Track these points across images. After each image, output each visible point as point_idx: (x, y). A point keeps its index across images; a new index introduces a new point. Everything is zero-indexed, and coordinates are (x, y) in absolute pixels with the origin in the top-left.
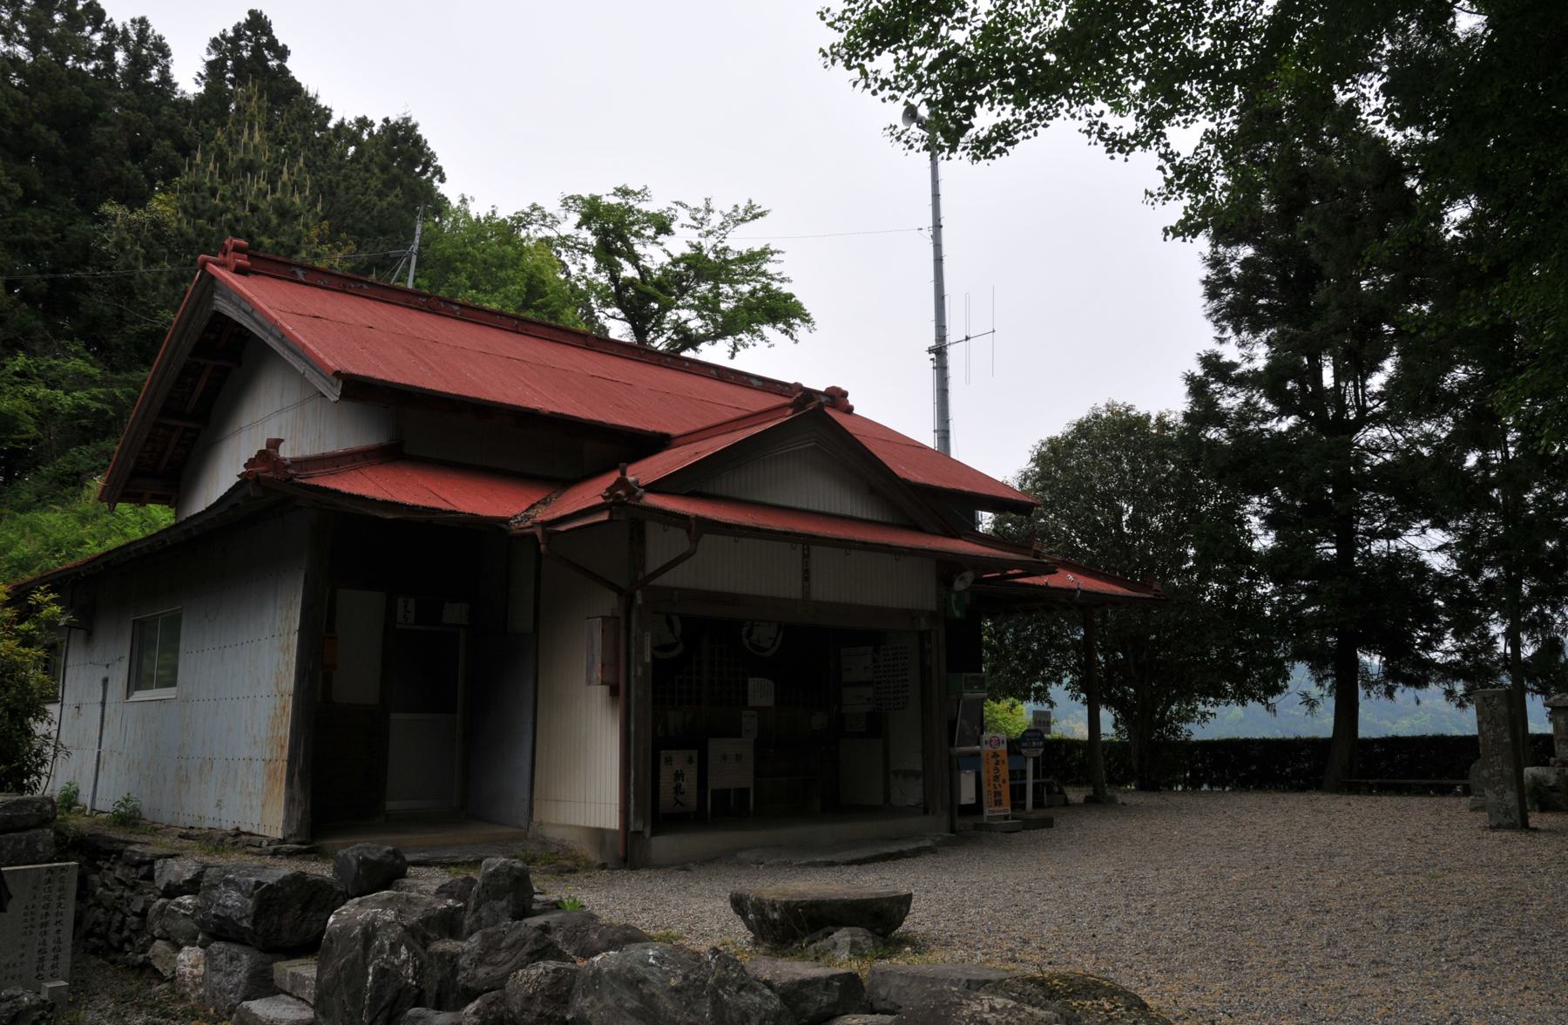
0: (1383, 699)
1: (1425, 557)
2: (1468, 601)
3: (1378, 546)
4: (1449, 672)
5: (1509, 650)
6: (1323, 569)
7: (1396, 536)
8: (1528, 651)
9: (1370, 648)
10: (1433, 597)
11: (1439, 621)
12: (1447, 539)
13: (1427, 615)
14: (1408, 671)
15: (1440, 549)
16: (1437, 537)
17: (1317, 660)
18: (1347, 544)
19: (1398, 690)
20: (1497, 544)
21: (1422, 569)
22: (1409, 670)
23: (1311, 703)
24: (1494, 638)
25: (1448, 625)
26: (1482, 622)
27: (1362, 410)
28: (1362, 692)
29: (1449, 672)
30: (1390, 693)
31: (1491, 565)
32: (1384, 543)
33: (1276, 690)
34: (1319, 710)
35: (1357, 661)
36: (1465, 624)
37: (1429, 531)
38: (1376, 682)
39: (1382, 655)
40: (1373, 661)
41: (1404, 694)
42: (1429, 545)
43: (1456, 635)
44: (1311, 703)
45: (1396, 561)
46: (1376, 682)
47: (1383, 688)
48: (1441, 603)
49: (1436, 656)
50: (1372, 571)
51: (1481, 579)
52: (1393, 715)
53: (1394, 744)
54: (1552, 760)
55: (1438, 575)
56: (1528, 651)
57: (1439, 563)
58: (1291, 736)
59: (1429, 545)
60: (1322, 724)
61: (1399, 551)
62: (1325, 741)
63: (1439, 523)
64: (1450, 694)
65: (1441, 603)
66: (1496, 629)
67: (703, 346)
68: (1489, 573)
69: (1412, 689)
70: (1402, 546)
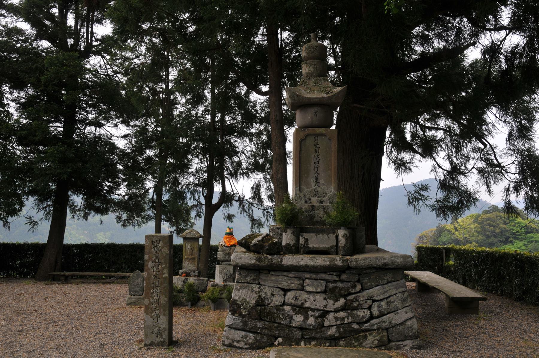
0: (81, 220)
1: (115, 140)
2: (136, 167)
3: (90, 129)
4: (121, 205)
5: (155, 197)
6: (51, 140)
7: (100, 125)
8: (166, 197)
9: (76, 191)
10: (117, 163)
11: (119, 178)
12: (128, 132)
13: (112, 174)
14: (97, 204)
15: (125, 137)
16: (124, 130)
17: (43, 196)
18: (70, 124)
19: (91, 215)
20: (155, 136)
21: (113, 146)
22: (98, 203)
23: (33, 223)
24: (148, 190)
25: (124, 180)
26: (141, 181)
27: (89, 46)
28: (69, 215)
29: (121, 205)
30: (86, 217)
31: (151, 148)
32: (93, 128)
33: (14, 212)
34: (39, 228)
35: (68, 197)
36: (134, 181)
37: (120, 126)
38: (79, 210)
39: (84, 195)
40: (78, 200)
41: (94, 218)
42: (118, 134)
43: (128, 186)
44: (33, 223)
45: (99, 139)
46: (79, 210)
47: (82, 213)
48: (121, 167)
49: (115, 197)
50: (83, 143)
51: (145, 156)
52: (85, 230)
53: (85, 249)
54: (181, 271)
55: (122, 151)
56: (166, 197)
57: (121, 144)
58: (22, 242)
59: (118, 134)
60: (41, 235)
61: (100, 135)
62: (46, 244)
63: (126, 122)
64: (119, 219)
65: (121, 167)
66: (150, 184)
67: (338, 283)
68: (150, 153)
69: (99, 215)
70: (103, 132)
